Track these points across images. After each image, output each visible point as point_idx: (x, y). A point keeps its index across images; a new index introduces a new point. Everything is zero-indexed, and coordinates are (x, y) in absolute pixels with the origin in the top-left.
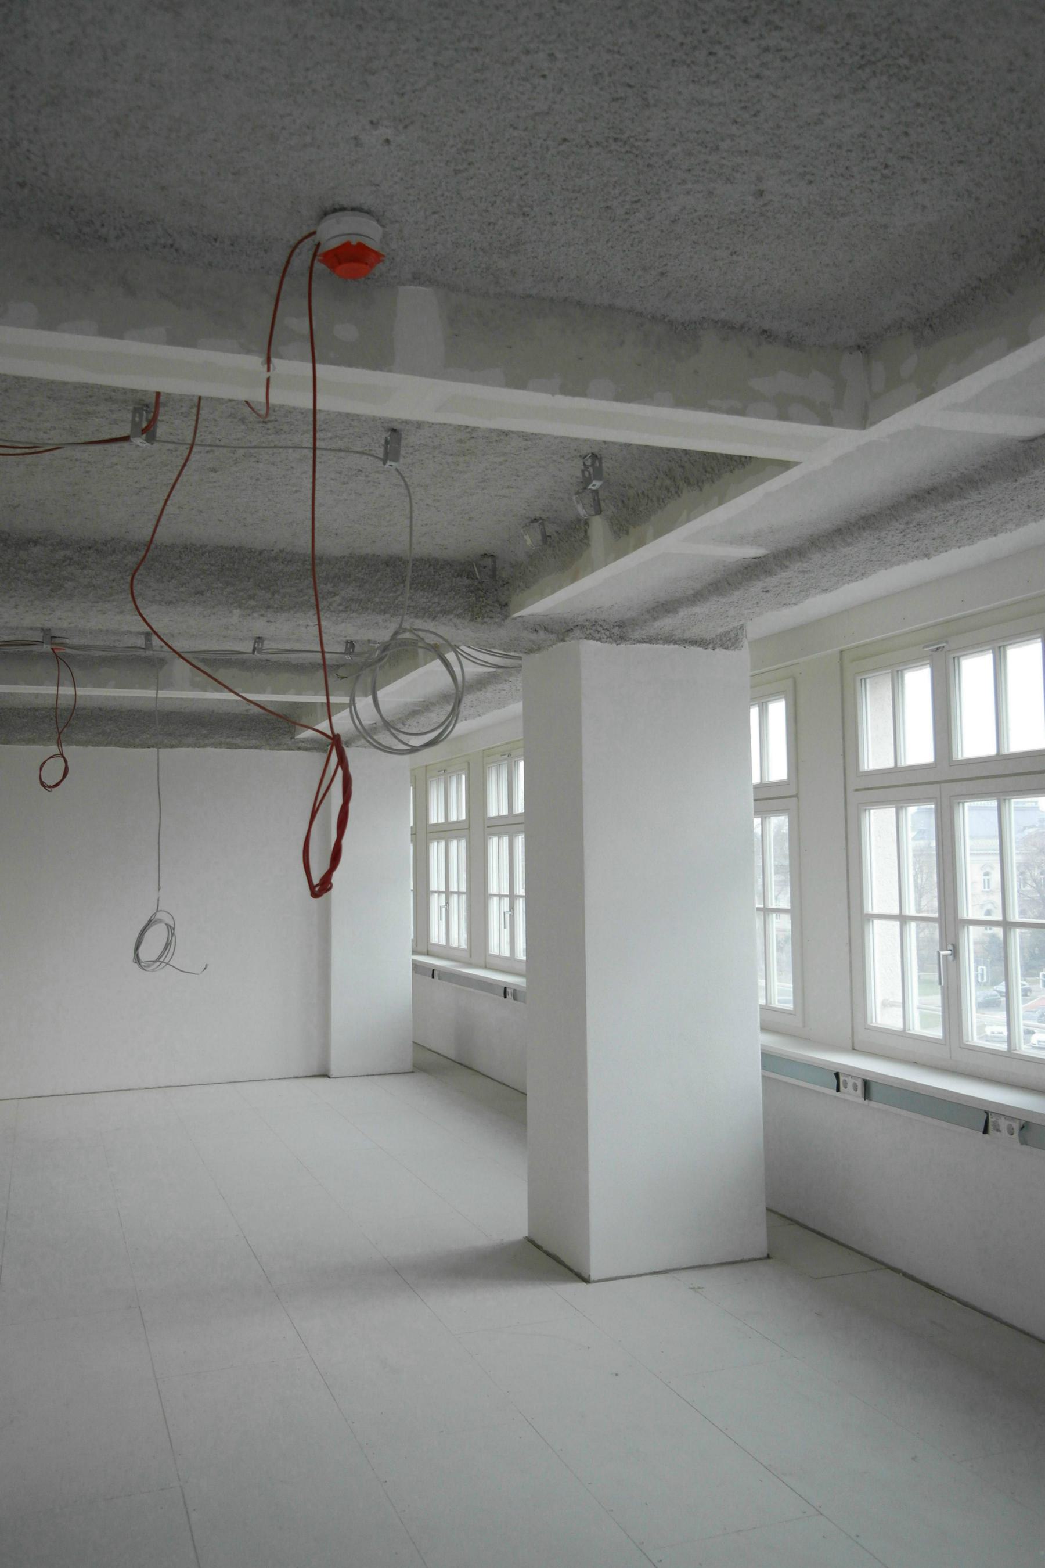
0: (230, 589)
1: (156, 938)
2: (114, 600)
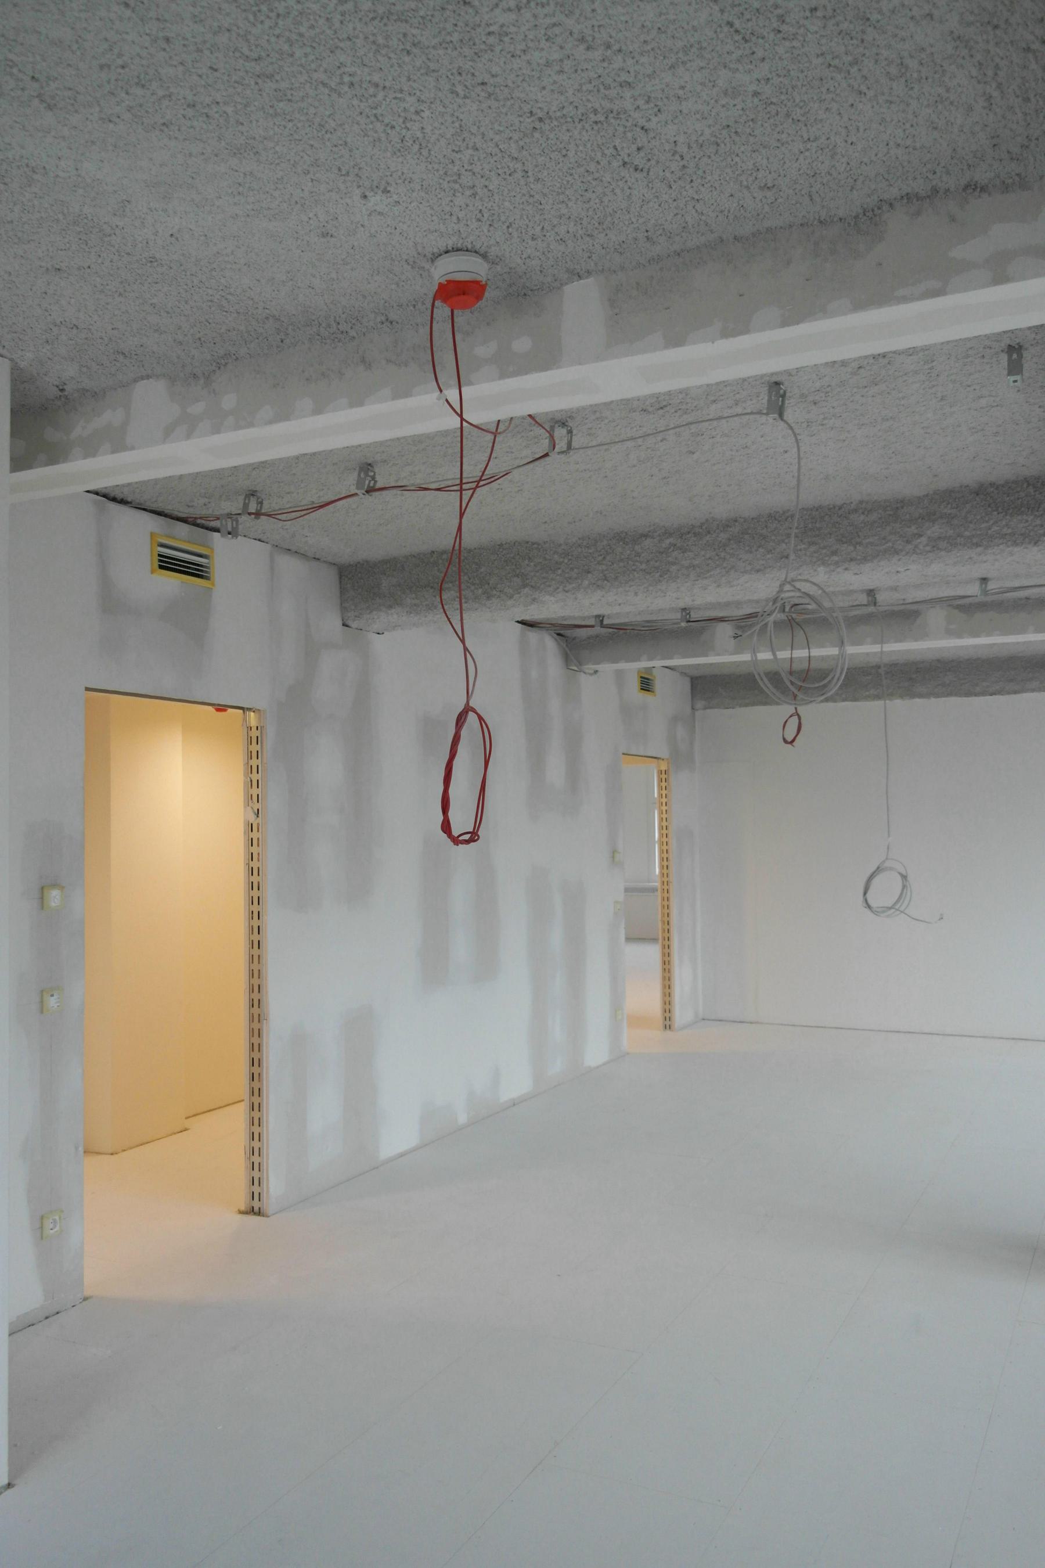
0: (813, 548)
1: (885, 890)
2: (711, 576)
